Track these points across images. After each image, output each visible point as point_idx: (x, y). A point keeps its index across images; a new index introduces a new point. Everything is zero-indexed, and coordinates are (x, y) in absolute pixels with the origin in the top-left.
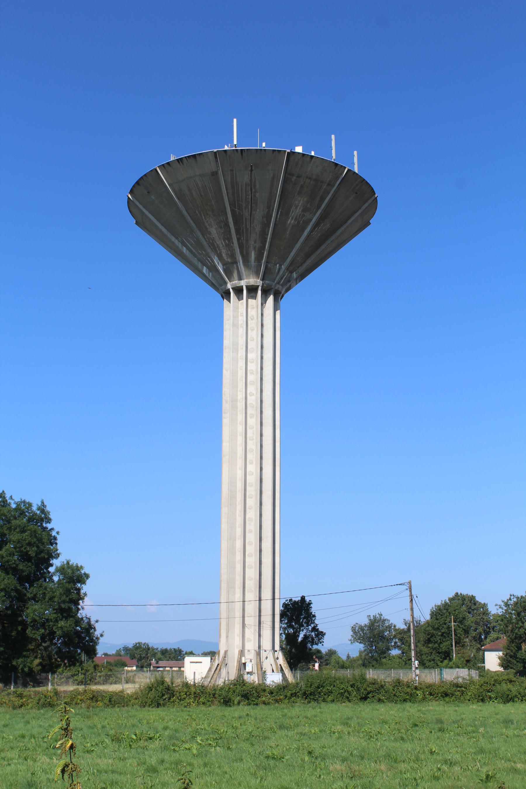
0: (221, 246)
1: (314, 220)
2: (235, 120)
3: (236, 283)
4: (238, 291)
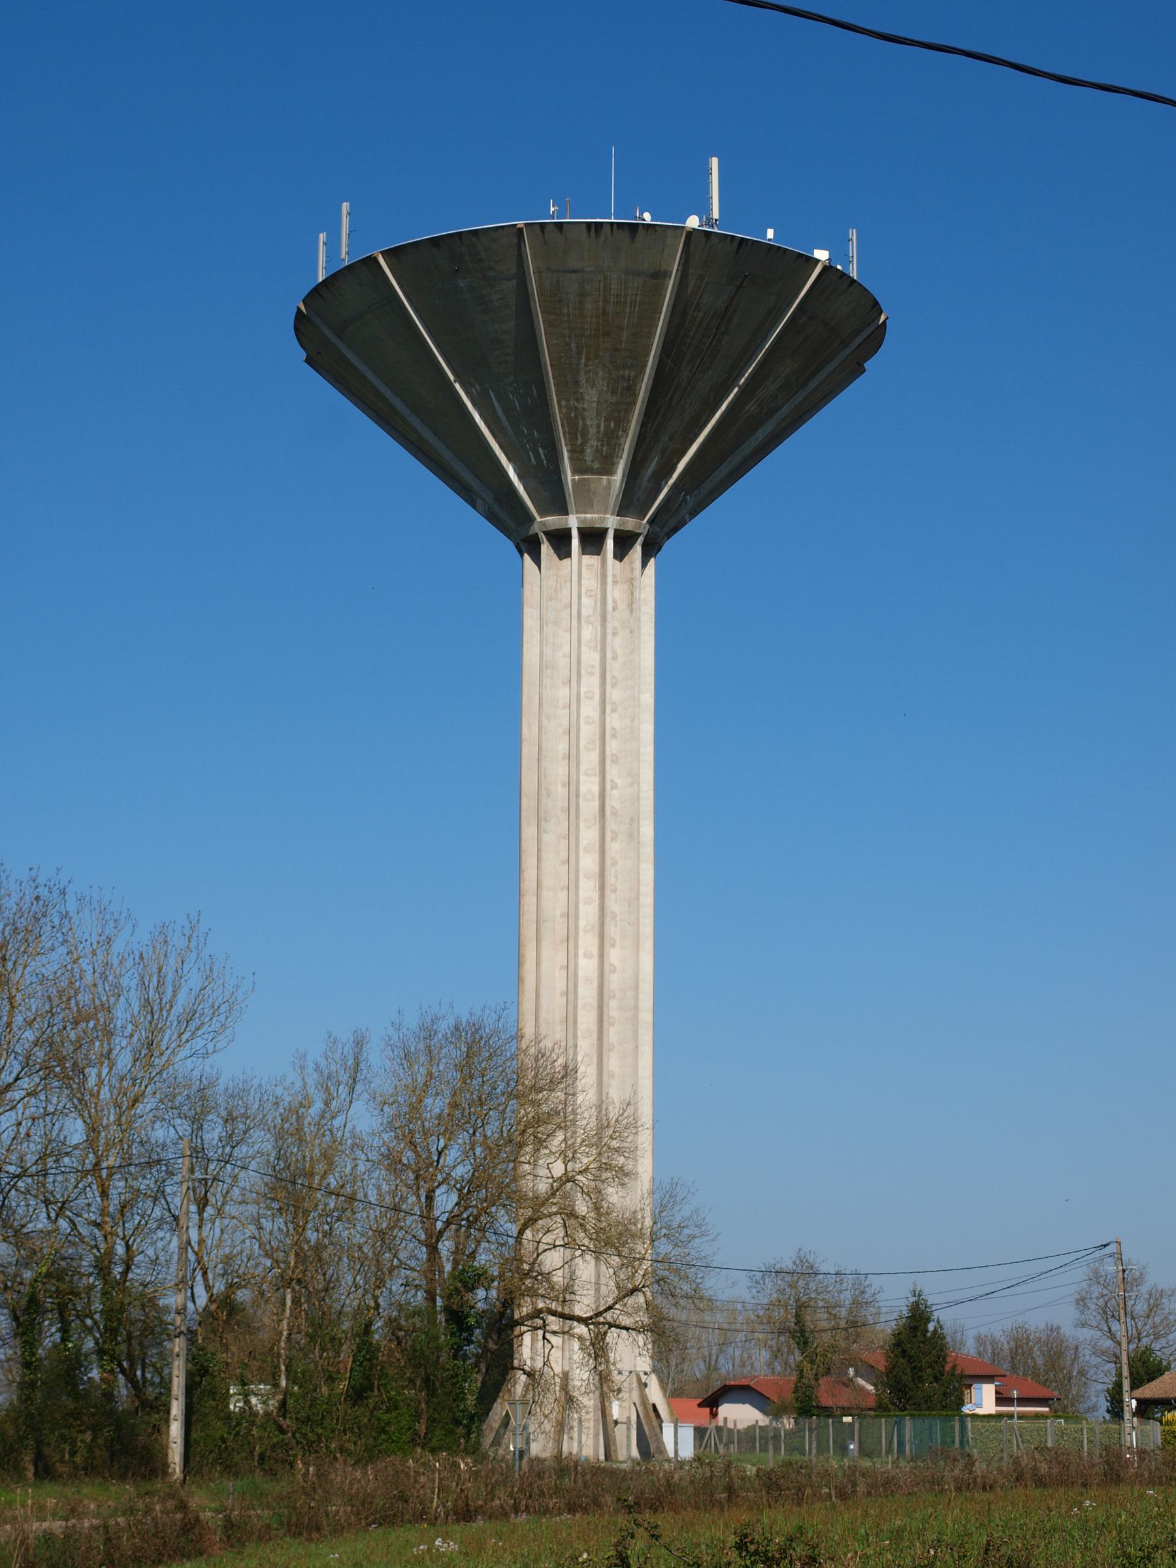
0: (593, 431)
1: (785, 410)
2: (715, 161)
3: (554, 521)
4: (560, 540)
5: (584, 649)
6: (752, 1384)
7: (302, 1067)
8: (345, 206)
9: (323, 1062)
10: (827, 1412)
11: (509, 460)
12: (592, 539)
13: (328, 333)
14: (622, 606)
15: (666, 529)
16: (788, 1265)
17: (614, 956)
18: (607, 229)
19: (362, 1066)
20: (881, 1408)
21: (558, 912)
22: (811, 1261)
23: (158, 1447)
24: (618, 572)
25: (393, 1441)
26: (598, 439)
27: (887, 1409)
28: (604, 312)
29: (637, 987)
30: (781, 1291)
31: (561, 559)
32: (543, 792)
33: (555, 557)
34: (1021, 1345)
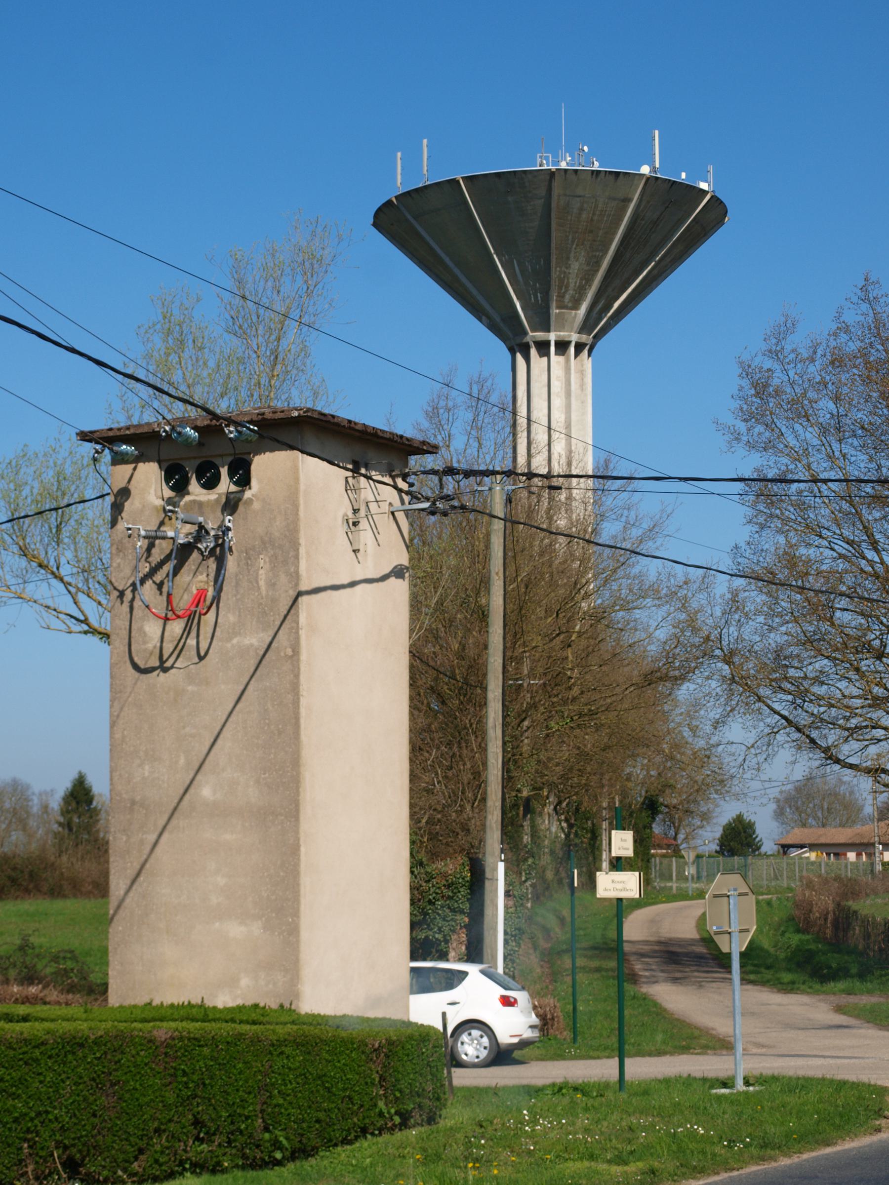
0: (572, 285)
3: (540, 335)
8: (425, 141)
11: (518, 299)
12: (562, 347)
13: (409, 216)
18: (603, 174)
31: (541, 357)
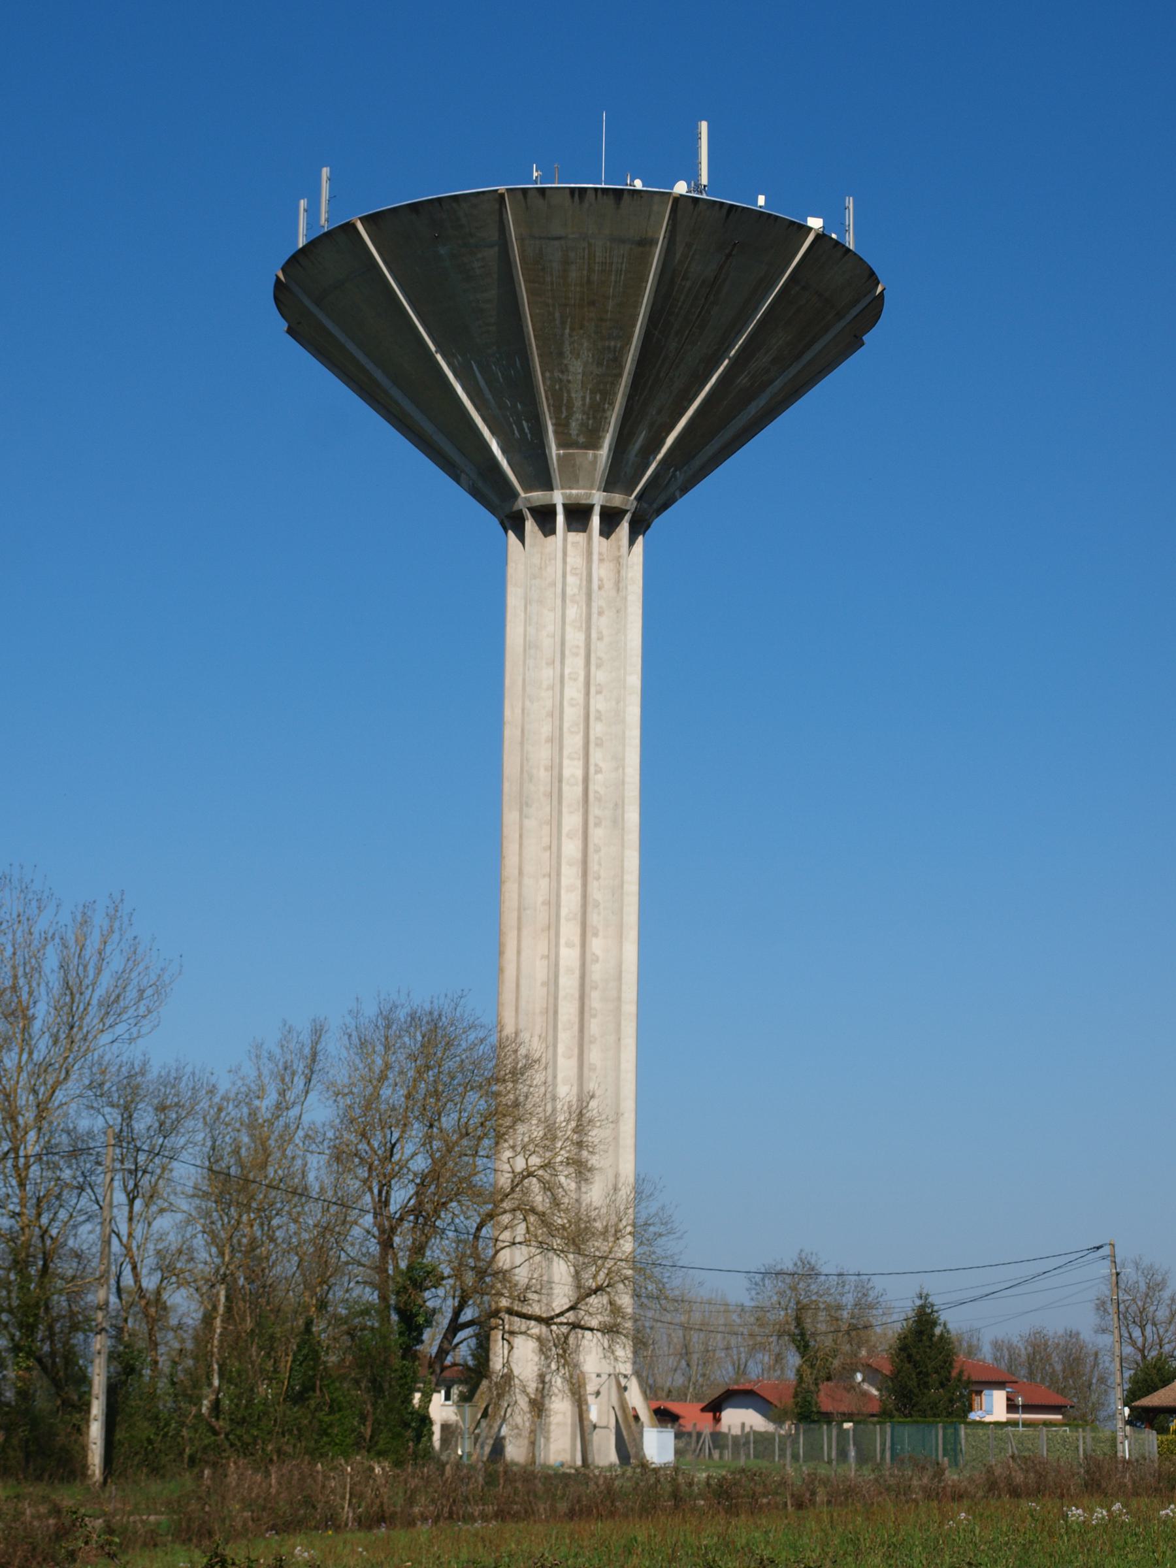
0: (578, 403)
1: (778, 384)
3: (538, 497)
5: (568, 628)
6: (755, 1388)
7: (258, 1057)
8: (325, 172)
9: (277, 1051)
10: (827, 1418)
11: (493, 433)
12: (578, 516)
13: (307, 302)
14: (609, 584)
15: (655, 506)
16: (789, 1266)
17: (597, 945)
18: (591, 195)
19: (320, 1057)
20: (885, 1415)
21: (540, 899)
22: (813, 1262)
23: (77, 1448)
24: (604, 550)
25: (336, 1444)
26: (584, 413)
27: (891, 1416)
28: (589, 282)
29: (620, 978)
30: (782, 1294)
31: (545, 536)
32: (525, 775)
33: (540, 534)
34: (1038, 1350)
